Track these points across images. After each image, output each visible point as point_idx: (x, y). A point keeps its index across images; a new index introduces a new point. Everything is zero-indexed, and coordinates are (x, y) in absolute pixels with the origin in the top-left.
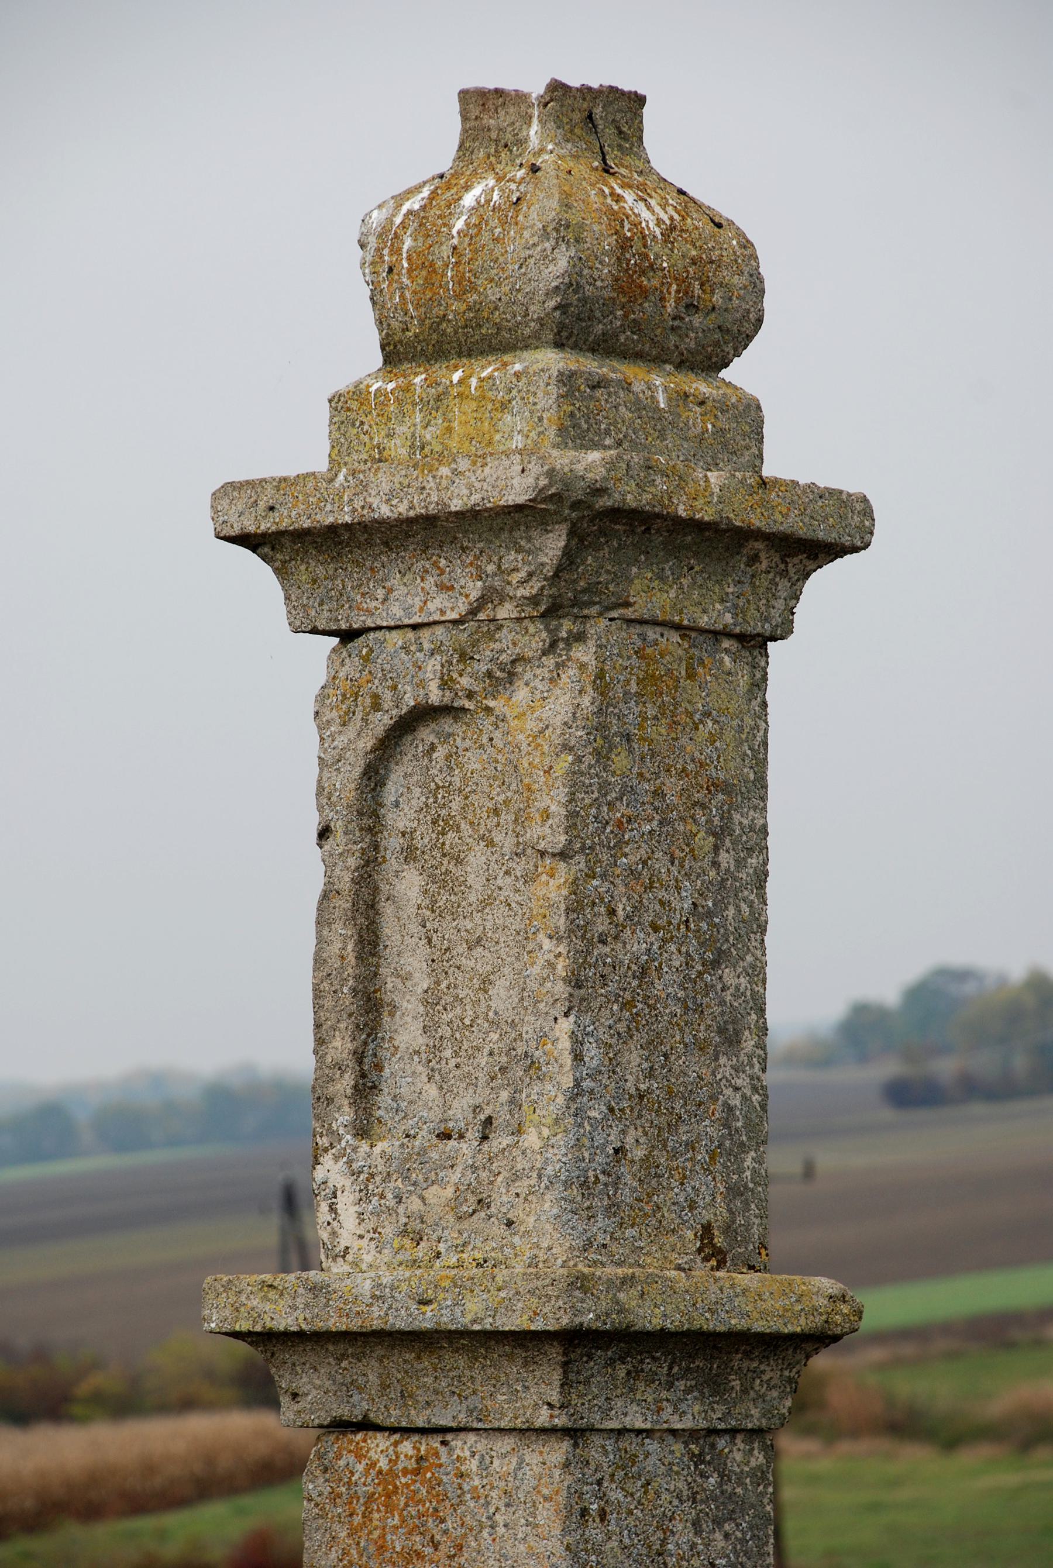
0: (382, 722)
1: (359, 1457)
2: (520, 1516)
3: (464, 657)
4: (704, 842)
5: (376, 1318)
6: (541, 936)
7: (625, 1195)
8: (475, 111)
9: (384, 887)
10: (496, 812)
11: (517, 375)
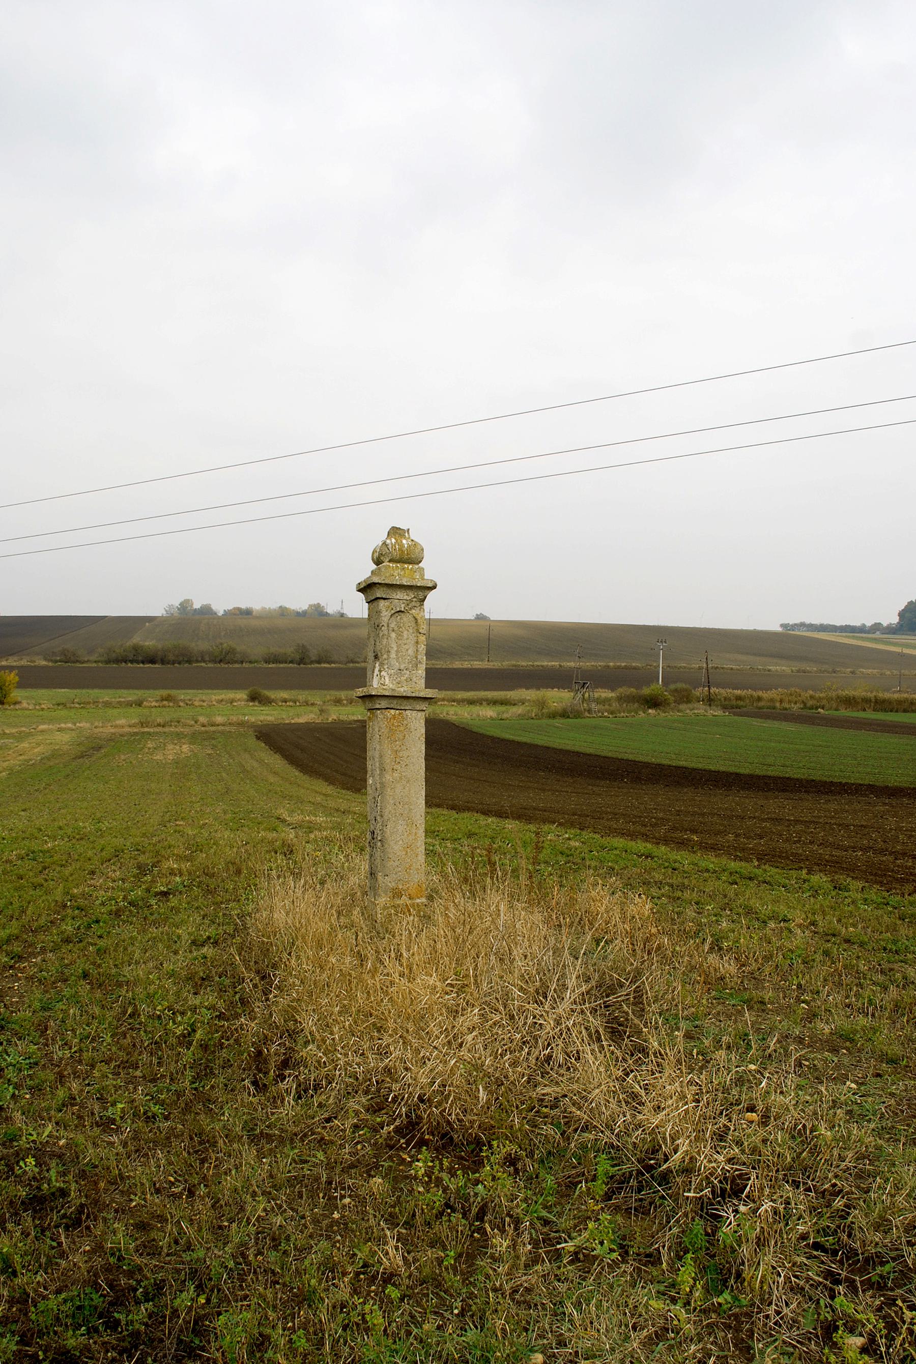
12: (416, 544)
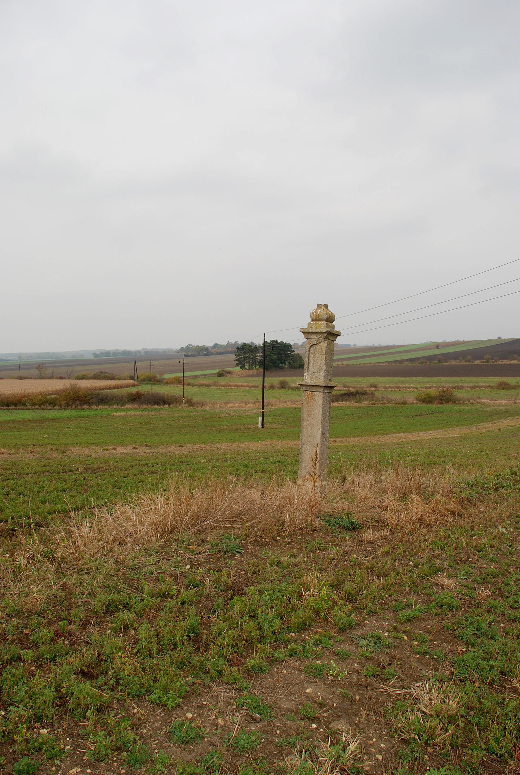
12: (332, 314)
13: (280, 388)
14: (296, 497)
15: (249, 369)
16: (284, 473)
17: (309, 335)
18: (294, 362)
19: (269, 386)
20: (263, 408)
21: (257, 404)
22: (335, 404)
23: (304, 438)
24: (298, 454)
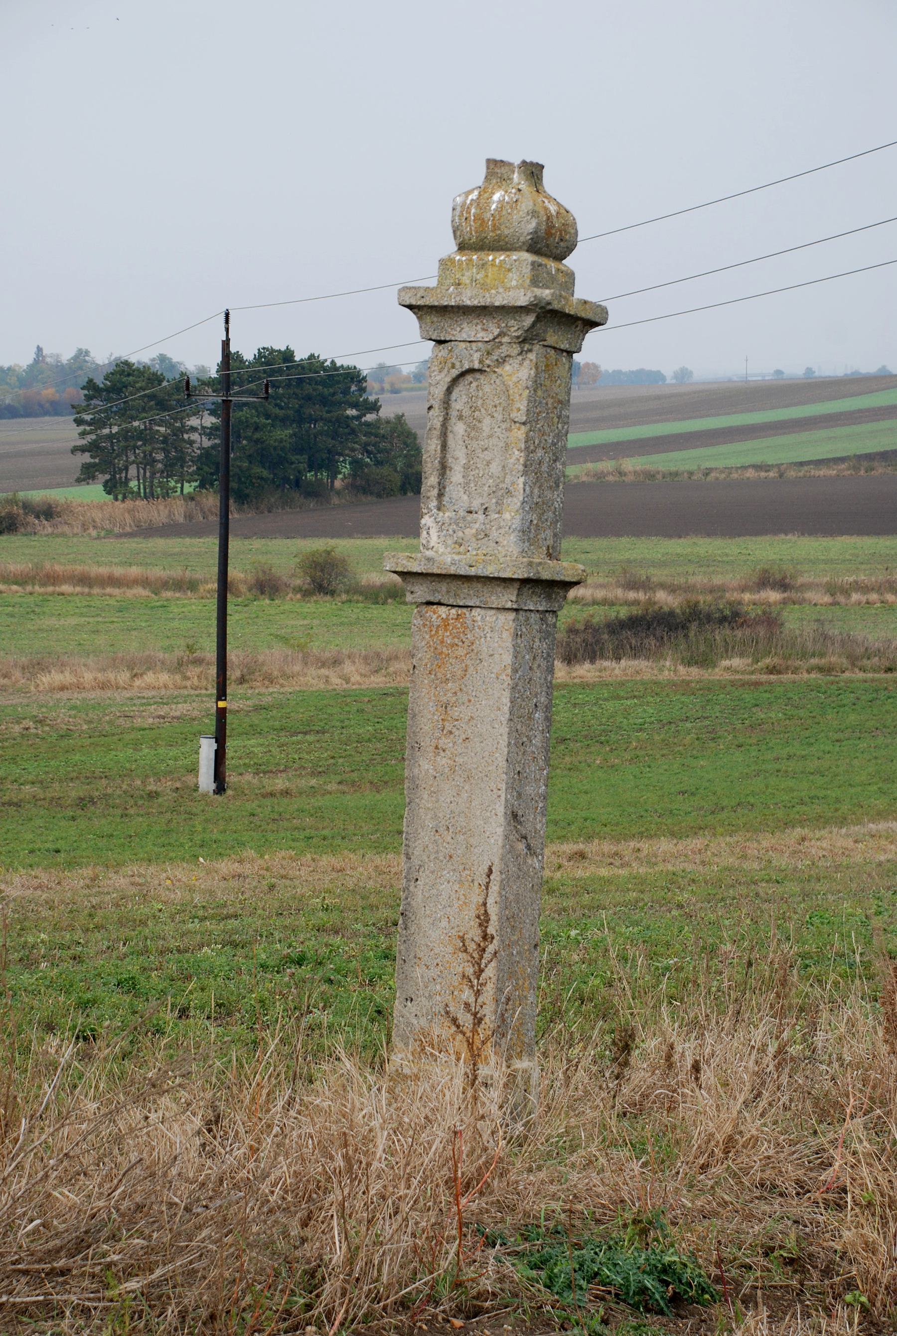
0: (455, 372)
1: (434, 613)
2: (496, 635)
3: (488, 353)
4: (556, 420)
5: (452, 570)
6: (514, 450)
7: (532, 536)
8: (492, 166)
9: (450, 428)
10: (496, 406)
11: (515, 261)
13: (306, 594)
14: (381, 1142)
15: (150, 496)
16: (325, 1018)
17: (445, 323)
18: (379, 463)
19: (251, 578)
20: (222, 694)
21: (193, 672)
22: (585, 671)
23: (423, 841)
24: (391, 923)
